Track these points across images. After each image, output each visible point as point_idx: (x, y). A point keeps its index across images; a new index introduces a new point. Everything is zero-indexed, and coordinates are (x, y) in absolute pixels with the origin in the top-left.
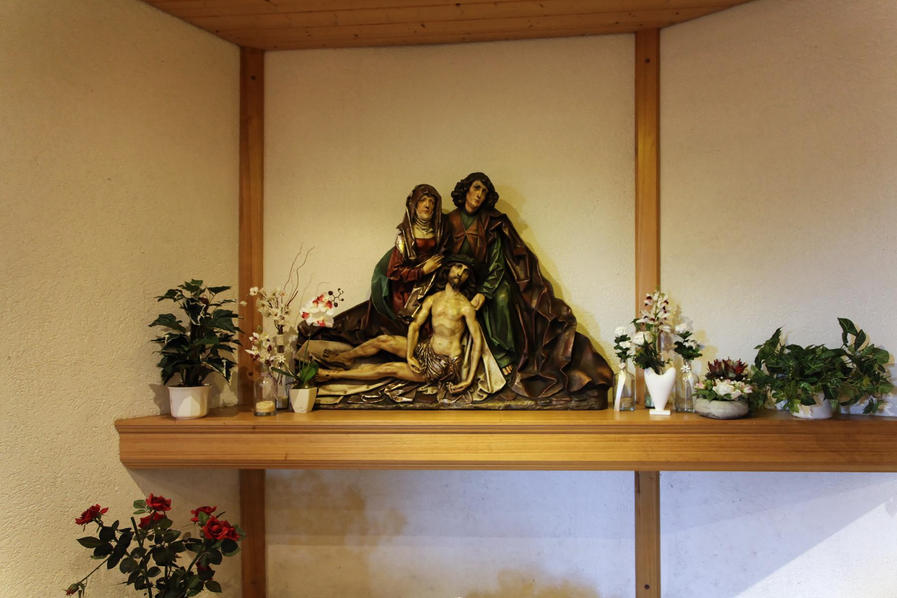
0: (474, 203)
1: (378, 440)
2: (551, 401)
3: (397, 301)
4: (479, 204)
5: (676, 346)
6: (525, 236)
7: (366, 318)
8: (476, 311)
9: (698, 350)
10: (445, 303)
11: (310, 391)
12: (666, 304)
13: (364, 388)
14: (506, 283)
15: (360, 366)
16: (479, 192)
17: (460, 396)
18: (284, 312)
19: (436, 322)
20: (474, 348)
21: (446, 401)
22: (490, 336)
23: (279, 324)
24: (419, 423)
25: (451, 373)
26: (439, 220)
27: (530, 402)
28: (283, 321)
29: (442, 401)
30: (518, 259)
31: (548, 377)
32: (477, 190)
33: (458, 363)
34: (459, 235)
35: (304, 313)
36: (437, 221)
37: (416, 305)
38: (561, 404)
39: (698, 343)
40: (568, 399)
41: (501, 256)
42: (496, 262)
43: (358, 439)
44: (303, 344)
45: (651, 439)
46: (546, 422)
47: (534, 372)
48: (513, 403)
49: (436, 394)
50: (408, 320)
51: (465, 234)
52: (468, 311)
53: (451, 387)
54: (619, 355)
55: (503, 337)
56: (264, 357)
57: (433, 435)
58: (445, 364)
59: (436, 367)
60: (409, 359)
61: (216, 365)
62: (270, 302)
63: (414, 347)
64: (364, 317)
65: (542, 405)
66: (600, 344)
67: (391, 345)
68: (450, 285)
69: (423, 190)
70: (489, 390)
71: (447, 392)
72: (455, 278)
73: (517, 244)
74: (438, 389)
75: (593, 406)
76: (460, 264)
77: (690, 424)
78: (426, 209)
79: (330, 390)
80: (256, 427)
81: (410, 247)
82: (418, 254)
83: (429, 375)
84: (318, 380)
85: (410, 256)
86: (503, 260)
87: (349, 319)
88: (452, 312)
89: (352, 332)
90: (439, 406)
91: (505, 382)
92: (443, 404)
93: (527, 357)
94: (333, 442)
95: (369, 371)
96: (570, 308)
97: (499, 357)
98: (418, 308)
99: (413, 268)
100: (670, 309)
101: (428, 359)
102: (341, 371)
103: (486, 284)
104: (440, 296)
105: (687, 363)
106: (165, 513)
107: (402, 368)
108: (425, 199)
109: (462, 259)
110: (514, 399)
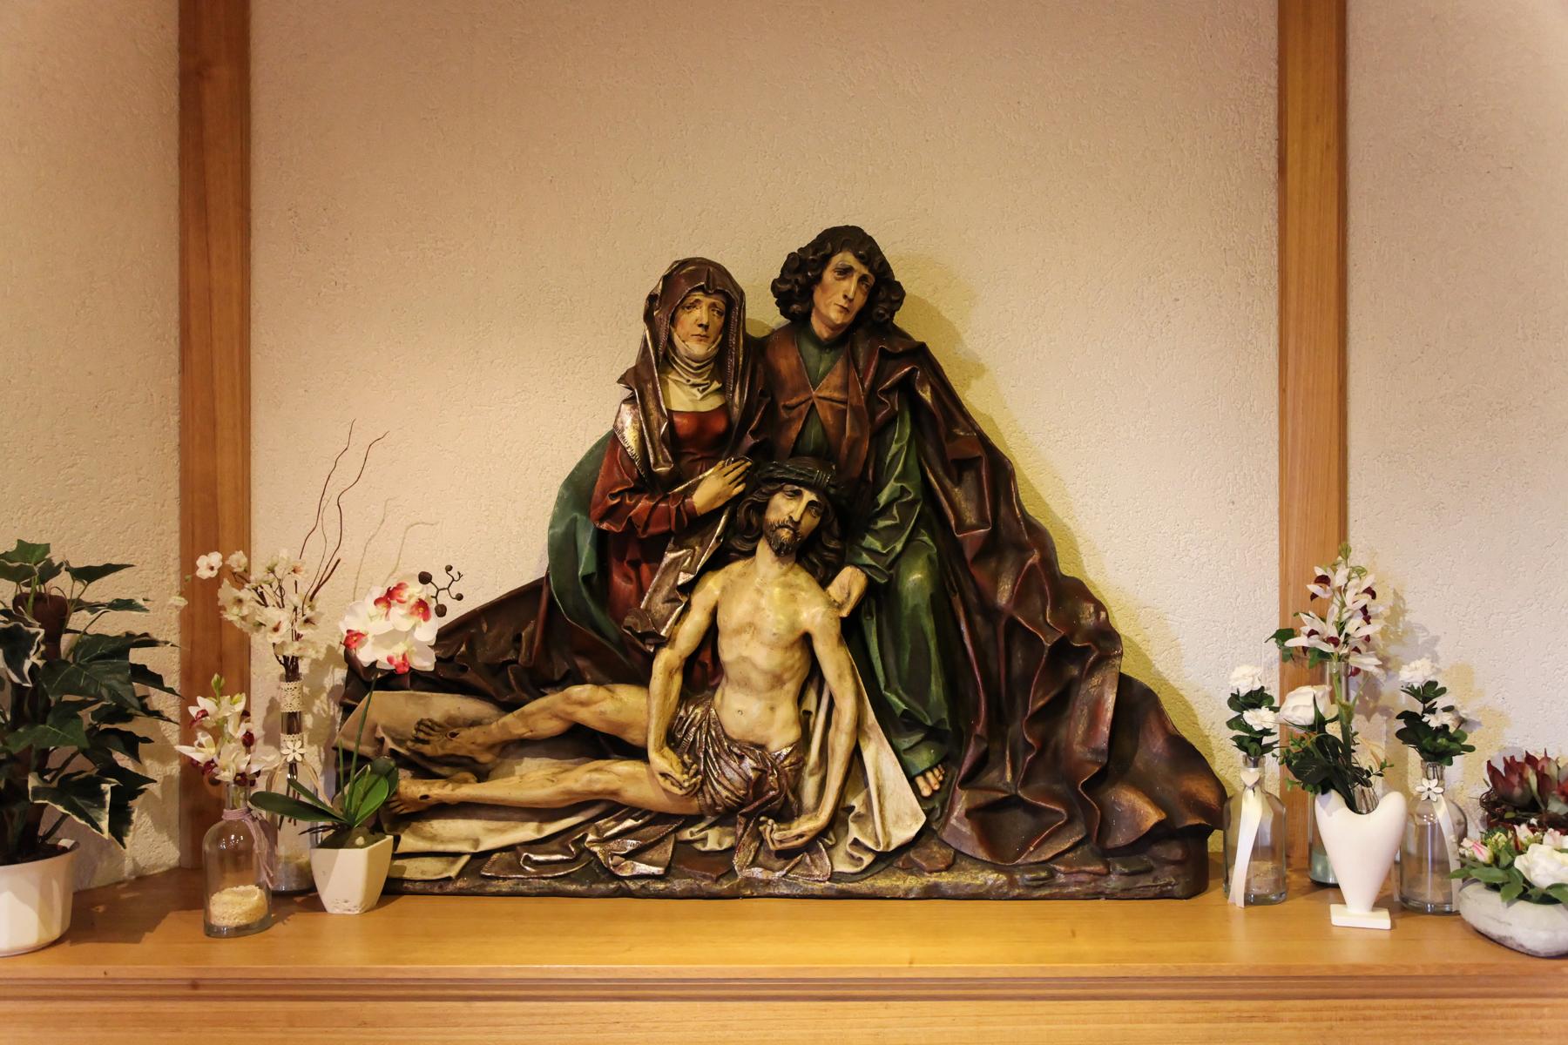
0: (835, 316)
1: (559, 1020)
2: (1052, 874)
3: (621, 584)
4: (849, 318)
5: (1401, 725)
6: (974, 398)
7: (535, 630)
8: (843, 620)
9: (1465, 737)
10: (754, 596)
11: (371, 856)
12: (1369, 596)
13: (528, 831)
14: (926, 538)
15: (519, 764)
16: (850, 285)
17: (799, 858)
18: (301, 619)
19: (729, 650)
20: (837, 724)
21: (757, 872)
22: (882, 686)
23: (286, 654)
24: (674, 971)
25: (772, 793)
26: (737, 357)
27: (996, 875)
28: (297, 644)
29: (747, 873)
30: (958, 468)
31: (1043, 804)
32: (844, 279)
33: (791, 764)
34: (794, 401)
35: (349, 631)
36: (731, 361)
37: (671, 600)
38: (1080, 883)
39: (1463, 713)
40: (1098, 868)
41: (912, 462)
42: (897, 480)
43: (500, 1015)
44: (359, 702)
45: (1341, 1014)
46: (1042, 968)
47: (1004, 788)
48: (946, 879)
49: (731, 850)
50: (651, 641)
51: (810, 399)
52: (819, 619)
53: (775, 834)
54: (1241, 743)
55: (917, 689)
56: (233, 766)
57: (716, 1004)
58: (754, 769)
59: (732, 775)
60: (652, 755)
61: (79, 802)
62: (260, 590)
63: (667, 719)
64: (529, 628)
65: (1027, 887)
66: (1182, 692)
67: (602, 713)
68: (767, 546)
69: (692, 277)
70: (878, 844)
71: (761, 844)
72: (783, 526)
73: (957, 425)
74: (735, 834)
75: (1169, 888)
76: (796, 488)
77: (1455, 972)
78: (700, 331)
79: (433, 838)
80: (201, 983)
81: (656, 436)
82: (677, 456)
83: (712, 796)
84: (398, 809)
85: (657, 464)
86: (918, 474)
87: (488, 630)
88: (774, 620)
89: (497, 669)
90: (738, 886)
91: (924, 818)
92: (750, 882)
93: (985, 745)
94: (427, 1026)
95: (543, 787)
96: (1104, 609)
97: (905, 743)
98: (679, 609)
99: (665, 498)
100: (1381, 609)
101: (706, 752)
102: (466, 781)
103: (871, 542)
104: (743, 575)
105: (1431, 774)
106: (309, 657)
107: (633, 778)
108: (697, 301)
109: (801, 475)
110: (948, 868)
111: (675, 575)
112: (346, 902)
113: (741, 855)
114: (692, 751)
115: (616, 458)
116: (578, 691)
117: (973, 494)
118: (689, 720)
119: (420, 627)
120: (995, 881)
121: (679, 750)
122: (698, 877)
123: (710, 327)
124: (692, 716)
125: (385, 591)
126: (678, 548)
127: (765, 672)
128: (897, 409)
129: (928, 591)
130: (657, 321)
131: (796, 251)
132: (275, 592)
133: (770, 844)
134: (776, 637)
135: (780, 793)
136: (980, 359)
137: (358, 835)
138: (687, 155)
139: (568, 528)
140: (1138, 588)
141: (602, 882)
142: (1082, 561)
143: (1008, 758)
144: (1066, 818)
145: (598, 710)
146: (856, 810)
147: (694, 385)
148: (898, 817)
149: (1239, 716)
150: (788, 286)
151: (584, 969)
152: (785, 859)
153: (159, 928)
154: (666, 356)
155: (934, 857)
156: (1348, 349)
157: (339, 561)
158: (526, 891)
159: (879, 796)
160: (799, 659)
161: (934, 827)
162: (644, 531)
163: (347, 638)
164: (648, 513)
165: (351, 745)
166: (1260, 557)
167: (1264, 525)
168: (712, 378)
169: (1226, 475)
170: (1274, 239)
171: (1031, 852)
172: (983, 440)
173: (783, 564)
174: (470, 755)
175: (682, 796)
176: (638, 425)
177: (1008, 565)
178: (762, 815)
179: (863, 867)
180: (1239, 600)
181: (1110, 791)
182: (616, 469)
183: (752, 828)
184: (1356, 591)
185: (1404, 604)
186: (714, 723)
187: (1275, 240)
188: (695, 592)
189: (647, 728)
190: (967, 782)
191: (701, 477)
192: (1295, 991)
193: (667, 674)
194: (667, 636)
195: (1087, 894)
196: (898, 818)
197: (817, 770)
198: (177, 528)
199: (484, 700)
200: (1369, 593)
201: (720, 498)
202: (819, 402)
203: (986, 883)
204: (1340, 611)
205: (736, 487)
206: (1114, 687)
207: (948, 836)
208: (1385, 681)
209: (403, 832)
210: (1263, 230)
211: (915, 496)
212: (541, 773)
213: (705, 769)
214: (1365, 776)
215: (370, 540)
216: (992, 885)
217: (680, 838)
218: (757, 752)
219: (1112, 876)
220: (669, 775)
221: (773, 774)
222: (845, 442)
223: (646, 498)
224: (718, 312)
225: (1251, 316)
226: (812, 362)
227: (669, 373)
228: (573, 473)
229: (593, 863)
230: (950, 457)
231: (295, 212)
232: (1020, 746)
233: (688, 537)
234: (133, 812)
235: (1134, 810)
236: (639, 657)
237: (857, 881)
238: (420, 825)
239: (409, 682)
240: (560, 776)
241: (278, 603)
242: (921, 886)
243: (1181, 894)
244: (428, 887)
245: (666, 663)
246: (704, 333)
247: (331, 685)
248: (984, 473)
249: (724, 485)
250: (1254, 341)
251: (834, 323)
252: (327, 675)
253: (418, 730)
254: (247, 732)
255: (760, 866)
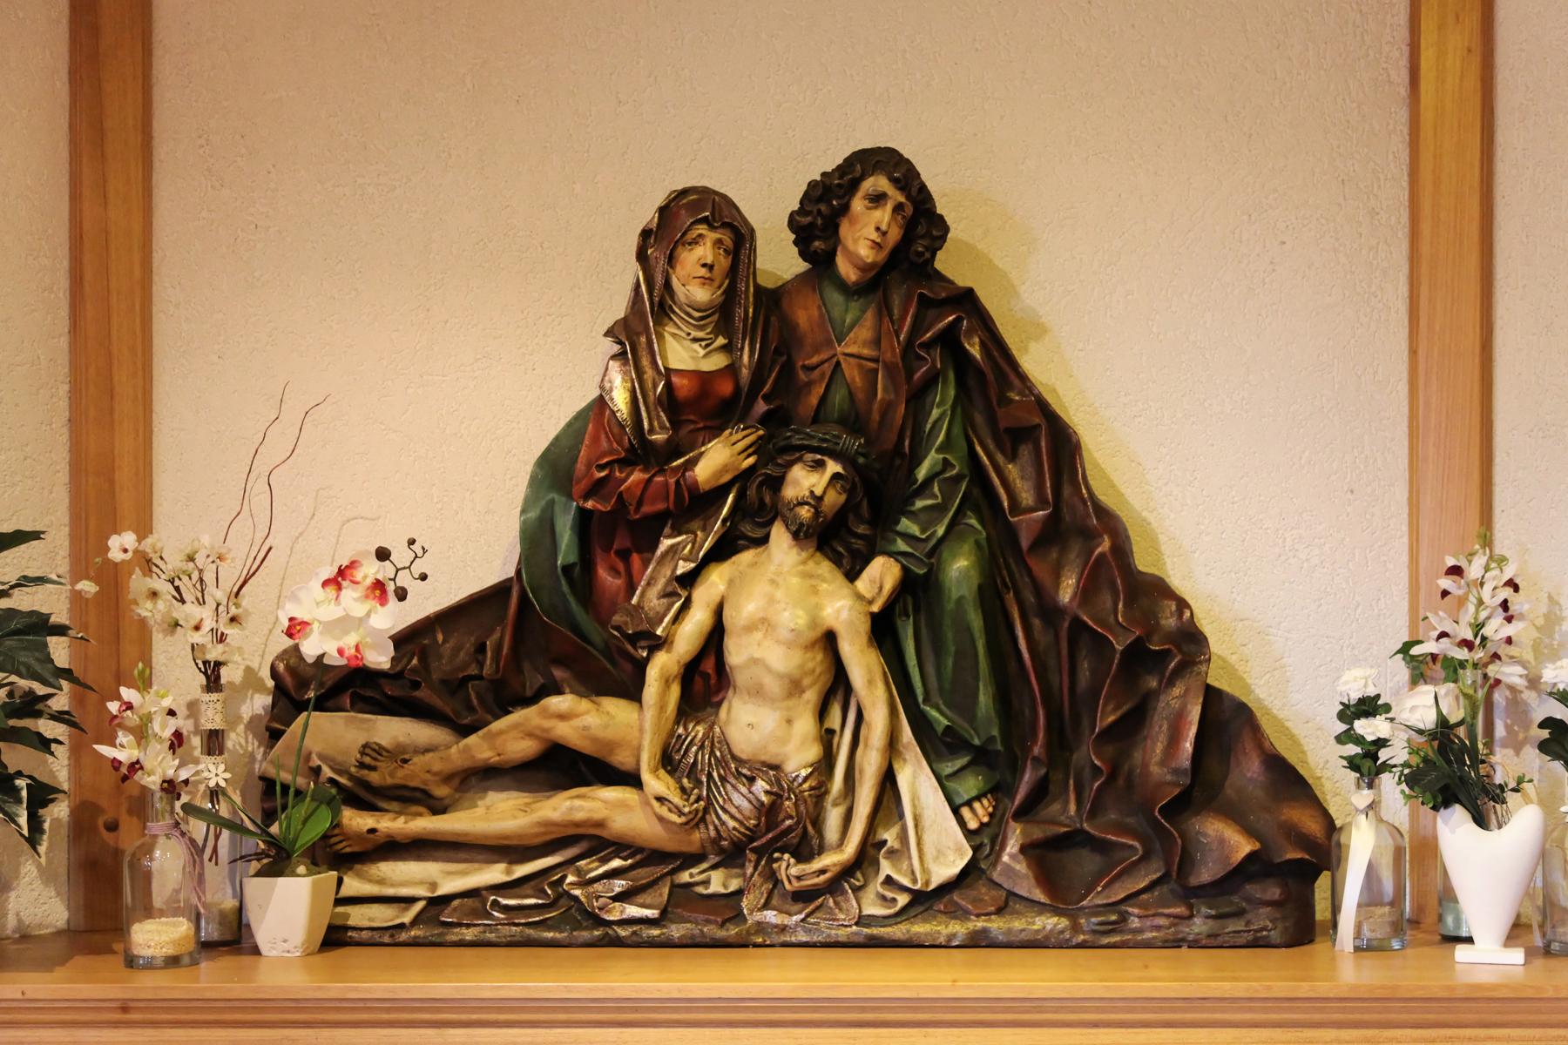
0: (865, 252)
2: (1124, 918)
3: (608, 579)
4: (882, 257)
5: (1545, 734)
6: (1035, 363)
10: (768, 588)
11: (315, 885)
12: (1511, 590)
13: (495, 874)
14: (973, 522)
16: (883, 215)
17: (820, 900)
19: (737, 652)
21: (771, 916)
22: (920, 699)
24: (680, 990)
25: (788, 822)
26: (746, 309)
28: (220, 647)
29: (758, 916)
30: (1013, 439)
32: (876, 208)
33: (812, 788)
34: (815, 360)
35: (291, 619)
36: (740, 312)
37: (669, 595)
38: (1158, 928)
40: (1180, 910)
41: (957, 430)
42: (939, 451)
47: (1067, 822)
48: (996, 925)
49: (739, 893)
50: (643, 643)
52: (845, 615)
53: (789, 869)
54: (1353, 764)
55: (962, 702)
57: (727, 1031)
58: (767, 792)
60: (646, 776)
62: (177, 583)
63: (664, 735)
64: (496, 636)
65: (1094, 932)
66: (1288, 724)
67: (585, 728)
68: (783, 529)
69: (695, 207)
70: (915, 881)
71: (775, 886)
73: (1011, 387)
75: (1265, 933)
78: (703, 272)
79: (381, 882)
81: (651, 398)
82: (675, 424)
84: (339, 846)
85: (652, 431)
87: (444, 641)
88: (792, 618)
89: (456, 686)
91: (970, 853)
92: (761, 927)
93: (1043, 771)
95: (515, 817)
96: (1188, 606)
97: (948, 768)
98: (678, 605)
99: (661, 471)
101: (710, 776)
102: (421, 815)
103: (906, 525)
104: (754, 565)
107: (622, 805)
108: (700, 236)
109: (825, 440)
110: (999, 911)
111: (672, 566)
112: (285, 941)
113: (751, 897)
114: (693, 776)
115: (603, 424)
116: (556, 702)
117: (1030, 470)
118: (689, 738)
119: (376, 613)
120: (1055, 925)
121: (678, 774)
122: (700, 921)
123: (715, 268)
124: (693, 734)
125: (336, 570)
126: (676, 533)
127: (780, 676)
128: (939, 366)
129: (975, 581)
130: (652, 262)
131: (819, 178)
132: (194, 585)
133: (786, 883)
134: (793, 633)
135: (798, 823)
136: (1041, 317)
137: (299, 863)
138: (683, 69)
139: (544, 511)
140: (1234, 595)
141: (586, 928)
142: (1165, 564)
143: (1072, 788)
144: (1140, 852)
145: (581, 725)
146: (889, 844)
147: (695, 340)
148: (939, 851)
149: (1349, 730)
150: (809, 219)
151: (575, 987)
152: (804, 902)
153: (67, 965)
154: (662, 304)
155: (982, 900)
156: (1494, 300)
157: (270, 549)
158: (495, 939)
159: (916, 826)
160: (822, 662)
161: (983, 866)
162: (637, 509)
163: (289, 628)
164: (641, 486)
165: (285, 776)
166: (1385, 558)
167: (1389, 519)
168: (717, 332)
169: (1343, 457)
170: (1404, 167)
171: (1098, 893)
172: (1043, 407)
173: (802, 551)
174: (423, 787)
175: (681, 824)
176: (629, 385)
177: (1072, 556)
178: (776, 850)
179: (897, 909)
180: (1359, 611)
181: (1194, 820)
182: (603, 436)
183: (764, 866)
184: (1494, 583)
185: (1561, 610)
186: (719, 742)
187: (1405, 169)
188: (696, 585)
189: (639, 749)
190: (1022, 814)
191: (703, 449)
192: (1404, 1017)
193: (663, 681)
194: (664, 635)
195: (1166, 941)
196: (940, 854)
197: (841, 800)
198: (66, 520)
199: (440, 725)
200: (1510, 586)
201: (727, 471)
202: (845, 360)
203: (1044, 928)
204: (1477, 611)
205: (746, 459)
206: (1198, 697)
207: (1000, 875)
208: (1538, 706)
209: (346, 873)
210: (1391, 157)
211: (960, 470)
212: (511, 803)
213: (708, 795)
214: (1498, 791)
215: (298, 538)
216: (1051, 930)
217: (677, 881)
218: (771, 773)
219: (1196, 919)
220: (667, 800)
221: (789, 798)
222: (876, 406)
223: (640, 470)
224: (725, 250)
225: (1375, 262)
226: (836, 312)
227: (666, 325)
228: (548, 450)
229: (574, 909)
230: (1002, 425)
231: (207, 140)
232: (1087, 772)
233: (691, 519)
234: (44, 821)
235: (1222, 841)
236: (628, 667)
237: (890, 926)
238: (365, 868)
239: (348, 701)
240: (534, 806)
241: (197, 599)
242: (966, 931)
243: (1278, 941)
244: (377, 936)
245: (662, 669)
246: (708, 275)
247: (250, 714)
248: (1043, 444)
249: (732, 456)
250: (1379, 293)
251: (864, 262)
252: (244, 701)
253: (363, 753)
254: (176, 731)
255: (773, 909)
